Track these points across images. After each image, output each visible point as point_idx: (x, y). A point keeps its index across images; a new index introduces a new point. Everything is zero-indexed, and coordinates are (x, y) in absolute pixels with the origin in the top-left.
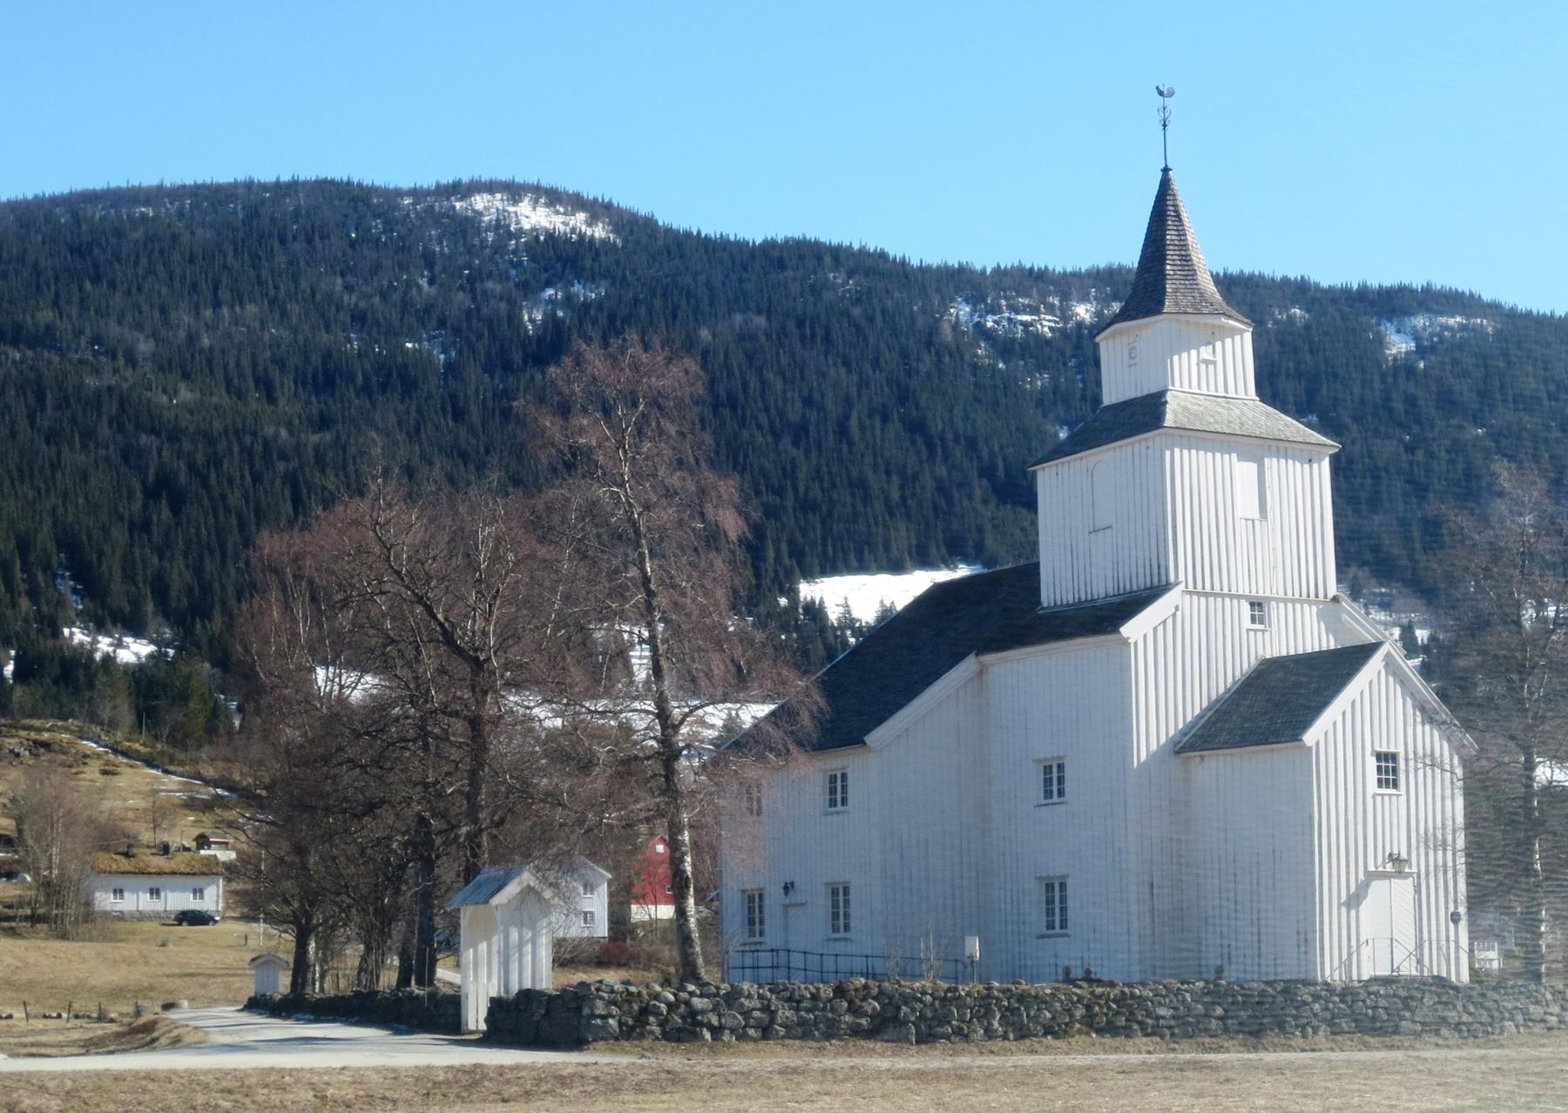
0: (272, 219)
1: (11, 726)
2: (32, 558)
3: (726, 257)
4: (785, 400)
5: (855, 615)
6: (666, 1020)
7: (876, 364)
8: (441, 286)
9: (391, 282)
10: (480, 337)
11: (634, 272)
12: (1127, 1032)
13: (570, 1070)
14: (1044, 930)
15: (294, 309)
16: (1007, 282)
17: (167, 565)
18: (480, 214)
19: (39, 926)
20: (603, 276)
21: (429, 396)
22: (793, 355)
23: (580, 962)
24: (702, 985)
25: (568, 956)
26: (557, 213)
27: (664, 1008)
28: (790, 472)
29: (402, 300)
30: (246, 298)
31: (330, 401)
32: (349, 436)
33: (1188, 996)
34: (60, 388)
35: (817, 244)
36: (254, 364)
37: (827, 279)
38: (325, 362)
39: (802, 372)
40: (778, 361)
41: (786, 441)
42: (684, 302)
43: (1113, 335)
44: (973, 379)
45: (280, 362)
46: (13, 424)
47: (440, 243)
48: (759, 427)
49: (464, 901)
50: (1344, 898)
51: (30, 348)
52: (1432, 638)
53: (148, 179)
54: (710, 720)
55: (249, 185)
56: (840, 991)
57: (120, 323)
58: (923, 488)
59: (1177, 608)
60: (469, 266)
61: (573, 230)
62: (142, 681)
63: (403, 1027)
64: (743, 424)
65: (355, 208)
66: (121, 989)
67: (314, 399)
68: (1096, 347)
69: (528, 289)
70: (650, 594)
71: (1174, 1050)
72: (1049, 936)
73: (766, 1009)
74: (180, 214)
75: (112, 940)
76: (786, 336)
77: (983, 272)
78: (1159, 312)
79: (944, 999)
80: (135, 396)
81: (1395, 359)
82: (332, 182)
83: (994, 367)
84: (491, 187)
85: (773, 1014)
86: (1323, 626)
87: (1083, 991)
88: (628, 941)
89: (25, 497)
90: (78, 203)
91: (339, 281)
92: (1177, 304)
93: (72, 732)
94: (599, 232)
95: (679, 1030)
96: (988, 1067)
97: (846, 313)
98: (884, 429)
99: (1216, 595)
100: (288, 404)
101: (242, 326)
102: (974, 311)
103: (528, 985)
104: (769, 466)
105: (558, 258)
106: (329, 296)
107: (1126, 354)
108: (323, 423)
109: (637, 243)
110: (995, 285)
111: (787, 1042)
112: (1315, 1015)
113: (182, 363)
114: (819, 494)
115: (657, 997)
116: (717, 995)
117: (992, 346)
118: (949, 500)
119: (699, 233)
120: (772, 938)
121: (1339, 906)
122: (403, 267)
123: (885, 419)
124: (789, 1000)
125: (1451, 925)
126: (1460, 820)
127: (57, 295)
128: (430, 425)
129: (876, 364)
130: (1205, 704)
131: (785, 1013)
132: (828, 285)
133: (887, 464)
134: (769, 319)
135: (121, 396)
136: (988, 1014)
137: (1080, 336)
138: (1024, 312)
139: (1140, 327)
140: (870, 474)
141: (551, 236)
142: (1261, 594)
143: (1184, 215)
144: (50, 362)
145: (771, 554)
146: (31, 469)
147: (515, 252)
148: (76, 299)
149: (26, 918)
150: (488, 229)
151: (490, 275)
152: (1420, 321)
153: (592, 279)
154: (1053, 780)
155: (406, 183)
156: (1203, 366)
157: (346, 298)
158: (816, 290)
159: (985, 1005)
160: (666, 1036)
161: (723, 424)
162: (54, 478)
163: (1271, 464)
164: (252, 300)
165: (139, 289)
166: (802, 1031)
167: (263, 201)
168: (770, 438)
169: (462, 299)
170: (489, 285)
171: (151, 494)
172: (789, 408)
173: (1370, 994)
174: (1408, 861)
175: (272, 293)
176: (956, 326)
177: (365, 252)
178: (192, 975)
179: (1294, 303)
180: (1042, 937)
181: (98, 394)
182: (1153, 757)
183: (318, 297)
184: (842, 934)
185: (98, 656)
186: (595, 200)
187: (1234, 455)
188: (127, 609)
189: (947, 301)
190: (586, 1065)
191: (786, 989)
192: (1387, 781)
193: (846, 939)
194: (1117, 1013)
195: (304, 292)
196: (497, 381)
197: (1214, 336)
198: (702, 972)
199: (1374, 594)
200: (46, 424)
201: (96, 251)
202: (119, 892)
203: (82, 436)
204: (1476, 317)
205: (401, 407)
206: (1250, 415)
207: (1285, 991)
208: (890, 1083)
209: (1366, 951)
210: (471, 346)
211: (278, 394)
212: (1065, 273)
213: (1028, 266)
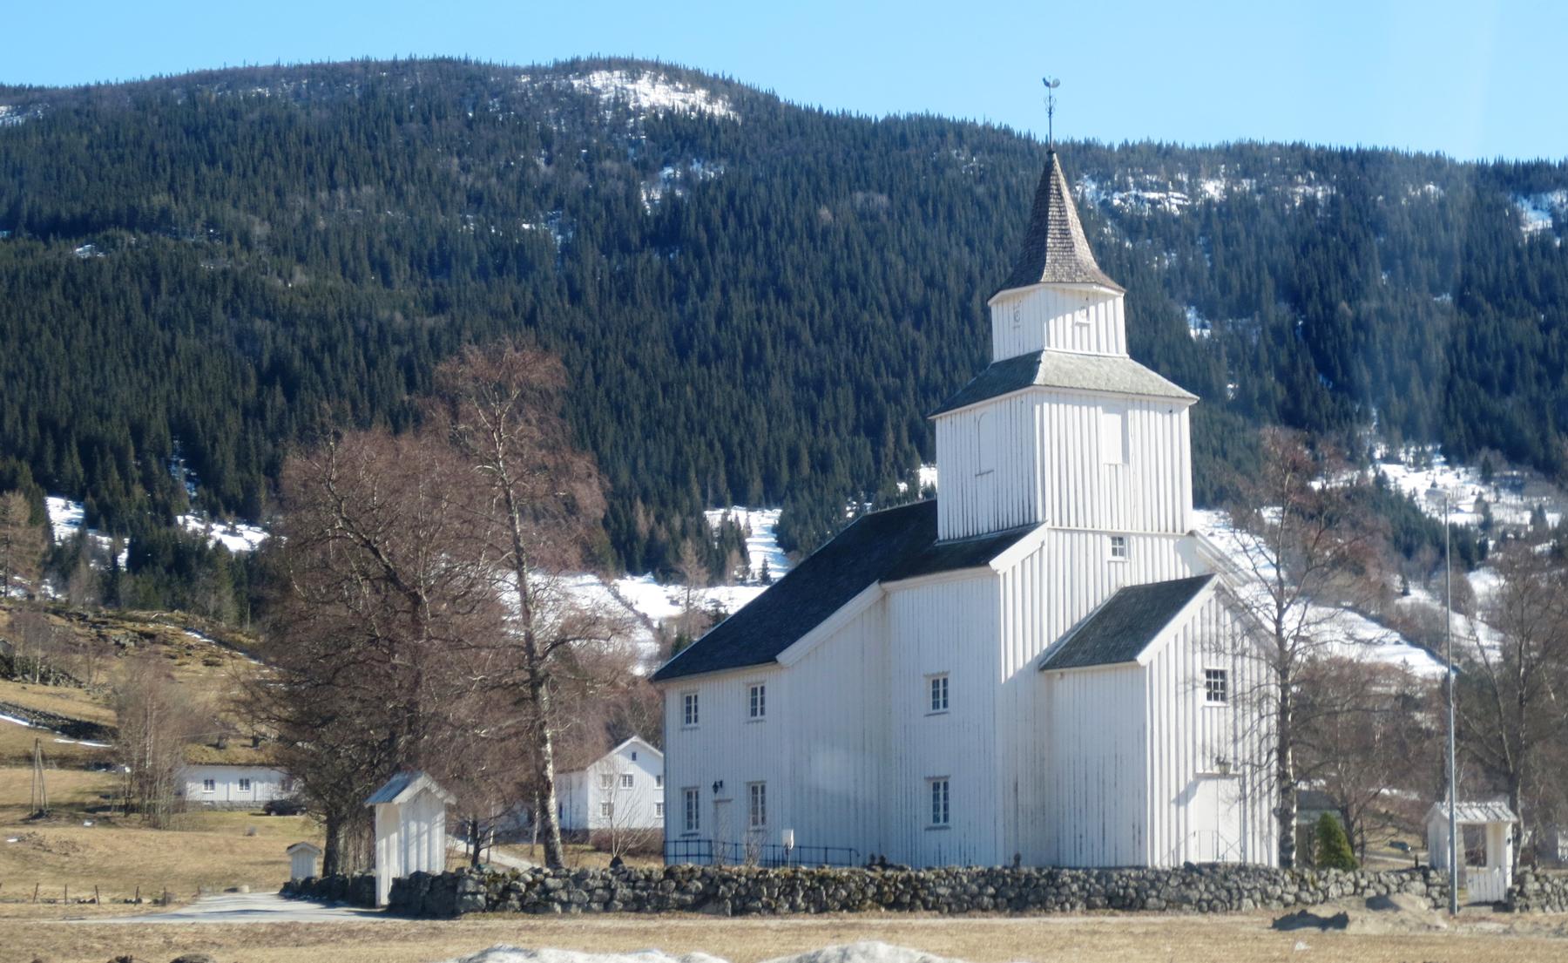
0: (389, 100)
1: (117, 618)
2: (146, 446)
3: (848, 135)
4: (906, 281)
7: (999, 242)
9: (508, 162)
11: (754, 150)
12: (911, 908)
14: (931, 824)
15: (411, 190)
16: (1135, 158)
17: (280, 451)
18: (599, 92)
19: (133, 816)
20: (722, 155)
21: (546, 279)
22: (914, 234)
23: (652, 852)
26: (677, 90)
27: (522, 886)
28: (910, 353)
30: (361, 180)
31: (446, 282)
32: (464, 319)
34: (175, 273)
35: (940, 120)
36: (370, 246)
37: (950, 157)
38: (440, 245)
39: (924, 253)
40: (900, 241)
41: (907, 322)
42: (804, 180)
43: (1001, 301)
45: (397, 245)
46: (127, 309)
47: (558, 122)
48: (880, 309)
50: (1173, 796)
51: (147, 231)
53: (265, 59)
55: (366, 65)
57: (235, 205)
60: (587, 145)
61: (693, 108)
62: (250, 567)
64: (863, 305)
65: (472, 87)
66: (206, 876)
67: (430, 282)
68: (987, 312)
69: (646, 169)
70: (519, 550)
74: (297, 94)
75: (201, 829)
76: (908, 214)
77: (1111, 147)
79: (756, 881)
80: (250, 281)
81: (1531, 237)
82: (449, 61)
83: (1120, 246)
84: (609, 65)
85: (613, 891)
87: (877, 874)
89: (140, 382)
90: (194, 84)
91: (456, 161)
93: (176, 623)
94: (719, 109)
97: (970, 190)
100: (405, 286)
101: (360, 207)
102: (1100, 188)
104: (889, 348)
105: (678, 136)
106: (446, 176)
108: (439, 306)
109: (757, 120)
113: (294, 247)
114: (940, 376)
117: (1120, 224)
119: (821, 109)
120: (705, 829)
121: (1169, 802)
122: (521, 147)
124: (627, 880)
127: (173, 178)
128: (546, 309)
129: (999, 242)
130: (1068, 627)
131: (623, 891)
134: (890, 197)
135: (235, 280)
136: (793, 891)
137: (1208, 215)
138: (1153, 190)
141: (669, 113)
144: (165, 246)
145: (891, 437)
146: (146, 354)
147: (634, 131)
148: (191, 183)
149: (121, 808)
150: (606, 107)
151: (608, 155)
153: (712, 156)
154: (939, 692)
155: (524, 63)
156: (1077, 328)
157: (462, 179)
158: (939, 169)
159: (791, 885)
161: (843, 306)
162: (168, 364)
163: (1135, 415)
164: (368, 181)
165: (255, 171)
166: (637, 906)
167: (380, 80)
168: (891, 320)
169: (579, 179)
170: (608, 164)
171: (266, 379)
172: (910, 289)
175: (388, 174)
177: (483, 132)
178: (275, 863)
180: (929, 829)
181: (213, 277)
182: (1020, 674)
183: (435, 178)
184: (760, 826)
185: (211, 544)
186: (716, 76)
187: (1100, 409)
188: (241, 497)
194: (903, 892)
195: (420, 173)
197: (1087, 301)
199: (1506, 478)
200: (160, 310)
201: (212, 133)
202: (210, 783)
203: (196, 321)
205: (517, 290)
209: (1193, 842)
211: (394, 277)
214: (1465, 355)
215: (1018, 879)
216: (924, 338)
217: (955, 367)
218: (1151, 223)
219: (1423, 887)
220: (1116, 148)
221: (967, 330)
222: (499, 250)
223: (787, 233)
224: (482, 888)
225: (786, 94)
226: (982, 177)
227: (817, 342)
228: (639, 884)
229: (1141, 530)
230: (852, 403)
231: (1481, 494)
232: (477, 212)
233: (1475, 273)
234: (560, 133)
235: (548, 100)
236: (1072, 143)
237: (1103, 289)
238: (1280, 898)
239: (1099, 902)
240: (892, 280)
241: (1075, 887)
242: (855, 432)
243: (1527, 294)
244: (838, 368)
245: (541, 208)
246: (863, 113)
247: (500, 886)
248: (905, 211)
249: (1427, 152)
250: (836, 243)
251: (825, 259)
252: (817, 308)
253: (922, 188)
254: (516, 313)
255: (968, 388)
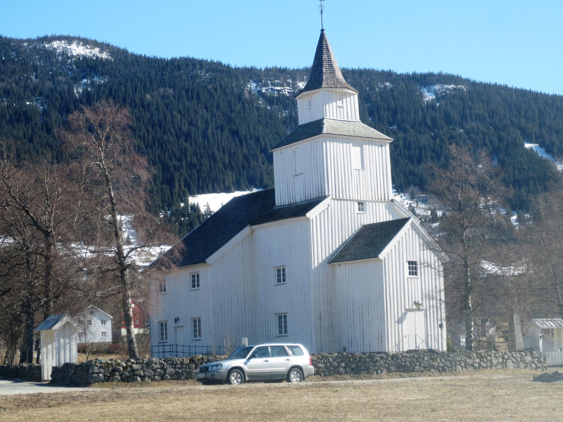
3: (156, 65)
4: (181, 123)
5: (212, 209)
6: (123, 374)
7: (218, 107)
8: (40, 79)
10: (57, 99)
11: (119, 72)
13: (77, 394)
16: (271, 73)
18: (56, 49)
20: (106, 74)
21: (37, 124)
22: (184, 105)
23: (100, 352)
24: (137, 359)
25: (95, 350)
26: (87, 48)
28: (184, 152)
29: (25, 85)
33: (331, 359)
35: (193, 59)
40: (178, 107)
41: (182, 140)
42: (139, 84)
43: (302, 97)
44: (257, 113)
47: (40, 61)
48: (171, 134)
49: (42, 329)
50: (396, 319)
52: (444, 214)
54: (154, 253)
56: (192, 361)
58: (238, 157)
59: (329, 205)
60: (51, 70)
61: (94, 55)
63: (19, 380)
64: (164, 133)
65: (4, 47)
69: (76, 80)
70: (113, 204)
71: (325, 380)
72: (281, 337)
73: (163, 368)
76: (181, 97)
77: (261, 69)
78: (320, 87)
81: (427, 103)
83: (266, 108)
84: (60, 38)
86: (387, 211)
88: (120, 343)
92: (327, 84)
94: (104, 56)
95: (128, 377)
96: (244, 388)
97: (205, 87)
98: (208, 136)
99: (344, 200)
103: (68, 361)
104: (175, 150)
105: (88, 66)
107: (308, 105)
109: (120, 60)
110: (265, 75)
111: (171, 381)
112: (382, 365)
114: (196, 160)
115: (119, 364)
116: (143, 363)
117: (265, 100)
118: (249, 163)
119: (145, 56)
120: (171, 340)
123: (222, 130)
124: (172, 364)
125: (440, 329)
126: (442, 288)
128: (37, 136)
129: (218, 107)
130: (341, 244)
131: (170, 370)
132: (197, 76)
133: (223, 148)
134: (174, 90)
138: (278, 86)
139: (313, 93)
140: (216, 152)
141: (85, 57)
142: (362, 199)
143: (330, 48)
147: (70, 64)
150: (59, 55)
151: (60, 74)
152: (437, 87)
153: (102, 75)
154: (281, 275)
155: (25, 37)
156: (338, 109)
158: (193, 78)
160: (122, 380)
161: (156, 132)
163: (366, 147)
168: (176, 139)
169: (49, 84)
172: (183, 127)
173: (403, 357)
174: (422, 304)
176: (250, 92)
177: (9, 65)
179: (386, 81)
182: (320, 265)
184: (198, 338)
186: (103, 43)
187: (351, 144)
189: (245, 83)
190: (84, 392)
191: (170, 360)
192: (413, 272)
193: (199, 340)
196: (64, 117)
197: (342, 96)
198: (137, 354)
199: (420, 197)
204: (460, 85)
205: (25, 129)
206: (357, 128)
207: (370, 357)
208: (203, 395)
209: (405, 340)
210: (53, 104)
212: (294, 70)
213: (279, 67)
214: (403, 149)
215: (355, 359)
216: (189, 146)
217: (202, 157)
218: (278, 99)
219: (531, 358)
220: (263, 69)
221: (206, 143)
222: (17, 113)
223: (133, 105)
224: (102, 370)
225: (131, 50)
226: (210, 82)
227: (146, 148)
228: (178, 366)
229: (370, 199)
230: (161, 172)
231: (411, 203)
232: (7, 98)
233: (406, 117)
234: (40, 65)
235: (35, 53)
236: (246, 68)
237: (349, 91)
238: (472, 365)
239: (393, 369)
240: (175, 123)
241: (382, 362)
242: (163, 183)
243: (426, 125)
244: (155, 158)
245: (34, 96)
246: (162, 57)
247: (110, 369)
248: (180, 96)
249: (385, 70)
250: (153, 108)
251: (148, 115)
252: (146, 135)
253: (187, 87)
254: (25, 138)
255: (288, 137)
